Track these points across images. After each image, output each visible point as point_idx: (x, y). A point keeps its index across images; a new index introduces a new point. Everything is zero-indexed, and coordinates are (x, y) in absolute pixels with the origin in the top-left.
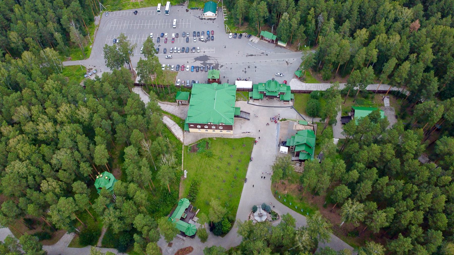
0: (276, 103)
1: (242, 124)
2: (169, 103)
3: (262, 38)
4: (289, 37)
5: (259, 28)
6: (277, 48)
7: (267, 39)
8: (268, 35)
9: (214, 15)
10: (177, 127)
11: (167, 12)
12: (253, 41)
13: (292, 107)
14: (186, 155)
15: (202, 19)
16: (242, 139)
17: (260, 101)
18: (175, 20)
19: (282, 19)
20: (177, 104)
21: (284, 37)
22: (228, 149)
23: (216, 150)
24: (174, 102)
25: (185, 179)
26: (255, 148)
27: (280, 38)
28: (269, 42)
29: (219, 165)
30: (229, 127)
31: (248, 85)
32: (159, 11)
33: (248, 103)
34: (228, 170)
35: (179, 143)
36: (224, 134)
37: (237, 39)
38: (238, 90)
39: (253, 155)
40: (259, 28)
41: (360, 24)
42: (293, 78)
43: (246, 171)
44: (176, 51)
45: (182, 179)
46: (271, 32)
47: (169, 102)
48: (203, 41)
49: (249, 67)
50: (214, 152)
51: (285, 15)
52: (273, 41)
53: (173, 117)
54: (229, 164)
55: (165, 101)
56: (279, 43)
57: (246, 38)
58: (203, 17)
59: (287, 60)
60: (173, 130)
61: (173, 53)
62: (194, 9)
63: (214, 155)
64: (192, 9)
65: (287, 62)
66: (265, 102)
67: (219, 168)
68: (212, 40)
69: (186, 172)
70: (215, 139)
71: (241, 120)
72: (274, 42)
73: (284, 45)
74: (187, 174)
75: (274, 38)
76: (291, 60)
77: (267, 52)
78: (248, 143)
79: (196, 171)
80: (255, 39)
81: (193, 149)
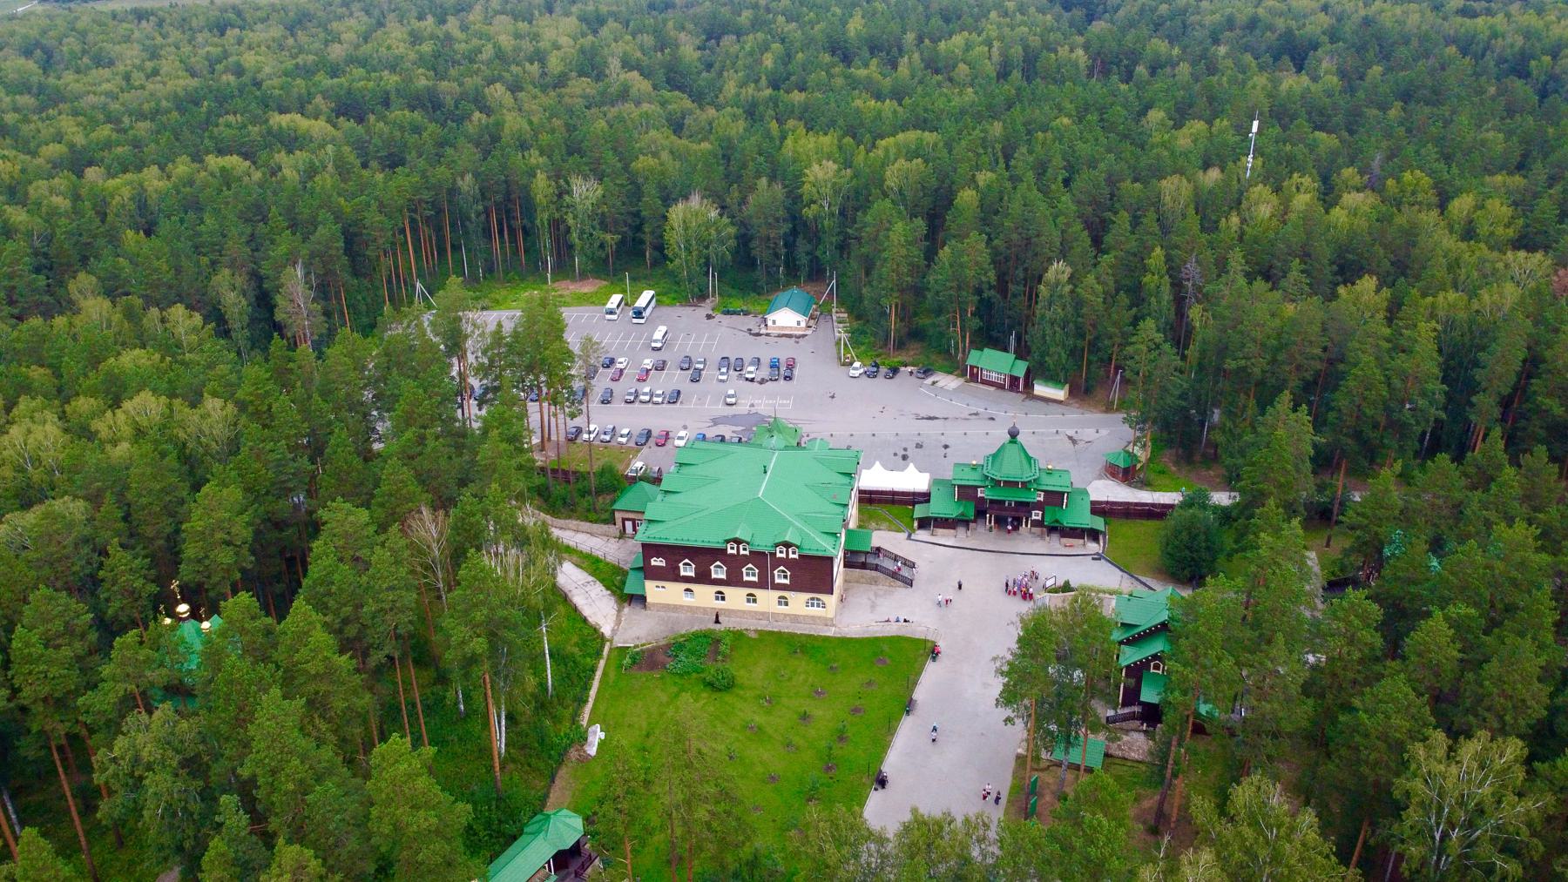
0: (1027, 540)
1: (876, 595)
2: (585, 525)
3: (974, 376)
4: (1074, 353)
5: (963, 338)
6: (1029, 403)
7: (994, 377)
8: (997, 363)
9: (803, 324)
10: (598, 590)
11: (639, 314)
12: (940, 384)
13: (1097, 557)
14: (612, 675)
15: (758, 335)
16: (874, 642)
17: (961, 530)
18: (663, 329)
19: (1047, 284)
20: (614, 530)
21: (1057, 355)
22: (805, 671)
23: (752, 672)
24: (605, 522)
25: (584, 759)
26: (932, 674)
27: (1042, 364)
28: (1000, 387)
29: (759, 719)
30: (812, 574)
31: (912, 480)
32: (611, 312)
33: (909, 537)
34: (796, 740)
35: (593, 638)
36: (795, 619)
37: (880, 380)
38: (869, 498)
39: (919, 694)
40: (963, 338)
41: (1332, 409)
42: (1100, 477)
43: (885, 747)
44: (647, 398)
45: (573, 754)
46: (1005, 350)
47: (587, 520)
48: (752, 380)
49: (919, 446)
50: (741, 675)
51: (1058, 270)
52: (1014, 380)
53: (592, 565)
54: (805, 717)
55: (570, 518)
56: (1040, 389)
57: (913, 379)
58: (763, 331)
59: (1071, 432)
60: (578, 600)
61: (637, 405)
62: (734, 313)
63: (742, 687)
64: (728, 313)
65: (1070, 438)
66: (983, 535)
67: (755, 731)
68: (788, 378)
69: (596, 735)
70: (753, 635)
71: (875, 582)
72: (1020, 386)
73: (1060, 394)
74: (602, 744)
75: (1020, 369)
76: (1088, 433)
77: (992, 412)
78: (903, 658)
79: (648, 736)
80: (949, 382)
81: (647, 660)
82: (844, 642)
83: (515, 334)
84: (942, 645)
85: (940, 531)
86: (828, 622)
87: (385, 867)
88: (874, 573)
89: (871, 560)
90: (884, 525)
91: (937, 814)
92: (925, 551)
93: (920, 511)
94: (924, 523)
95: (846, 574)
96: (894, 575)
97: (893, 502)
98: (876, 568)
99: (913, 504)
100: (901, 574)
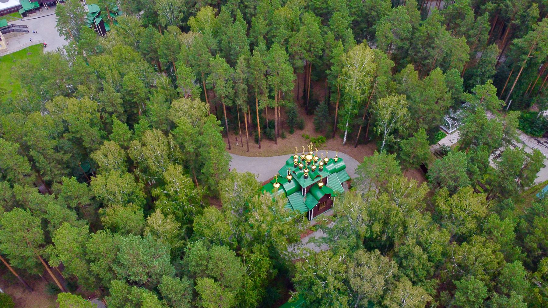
17: (38, 12)
71: (15, 35)
82: (14, 54)
83: (49, 56)
84: (46, 43)
85: (31, 15)
86: (5, 50)
87: (318, 302)
88: (14, 32)
89: (10, 29)
90: (11, 20)
91: (329, 141)
92: (30, 22)
93: (21, 11)
94: (24, 15)
95: (4, 36)
96: (21, 31)
97: (10, 12)
98: (14, 30)
99: (18, 10)
100: (24, 30)
